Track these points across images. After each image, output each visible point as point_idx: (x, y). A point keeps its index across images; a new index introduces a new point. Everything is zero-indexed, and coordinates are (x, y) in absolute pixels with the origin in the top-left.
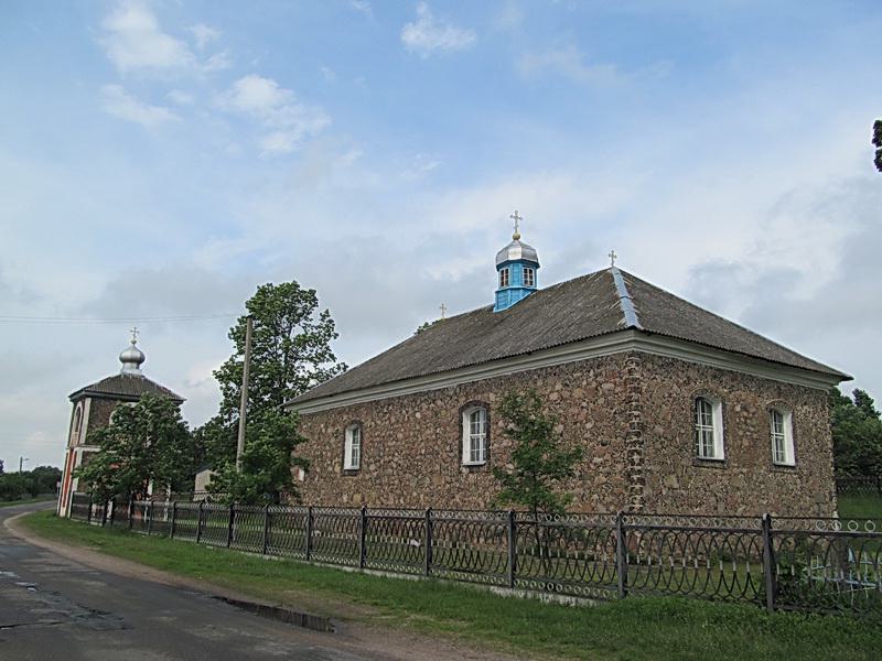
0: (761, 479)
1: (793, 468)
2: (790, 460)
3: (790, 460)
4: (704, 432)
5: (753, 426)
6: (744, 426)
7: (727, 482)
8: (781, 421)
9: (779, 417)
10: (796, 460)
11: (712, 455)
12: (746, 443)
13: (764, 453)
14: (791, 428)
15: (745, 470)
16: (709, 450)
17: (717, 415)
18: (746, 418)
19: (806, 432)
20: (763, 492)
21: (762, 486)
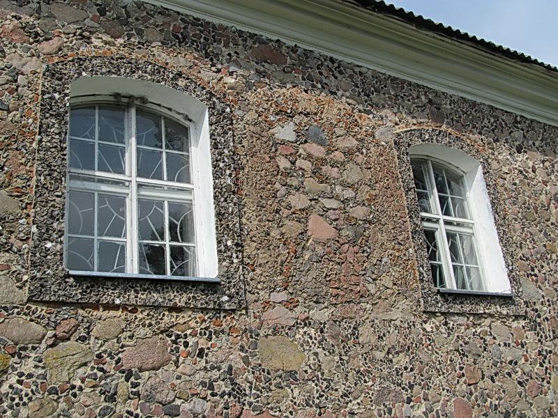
0: (392, 338)
1: (505, 299)
2: (495, 279)
3: (495, 279)
4: (468, 269)
5: (346, 185)
6: (310, 183)
7: (236, 359)
8: (184, 147)
9: (450, 182)
10: (513, 280)
11: (182, 270)
12: (320, 229)
13: (395, 261)
14: (486, 201)
15: (321, 314)
16: (114, 253)
17: (476, 197)
18: (319, 163)
19: (533, 213)
20: (407, 378)
21: (402, 360)
